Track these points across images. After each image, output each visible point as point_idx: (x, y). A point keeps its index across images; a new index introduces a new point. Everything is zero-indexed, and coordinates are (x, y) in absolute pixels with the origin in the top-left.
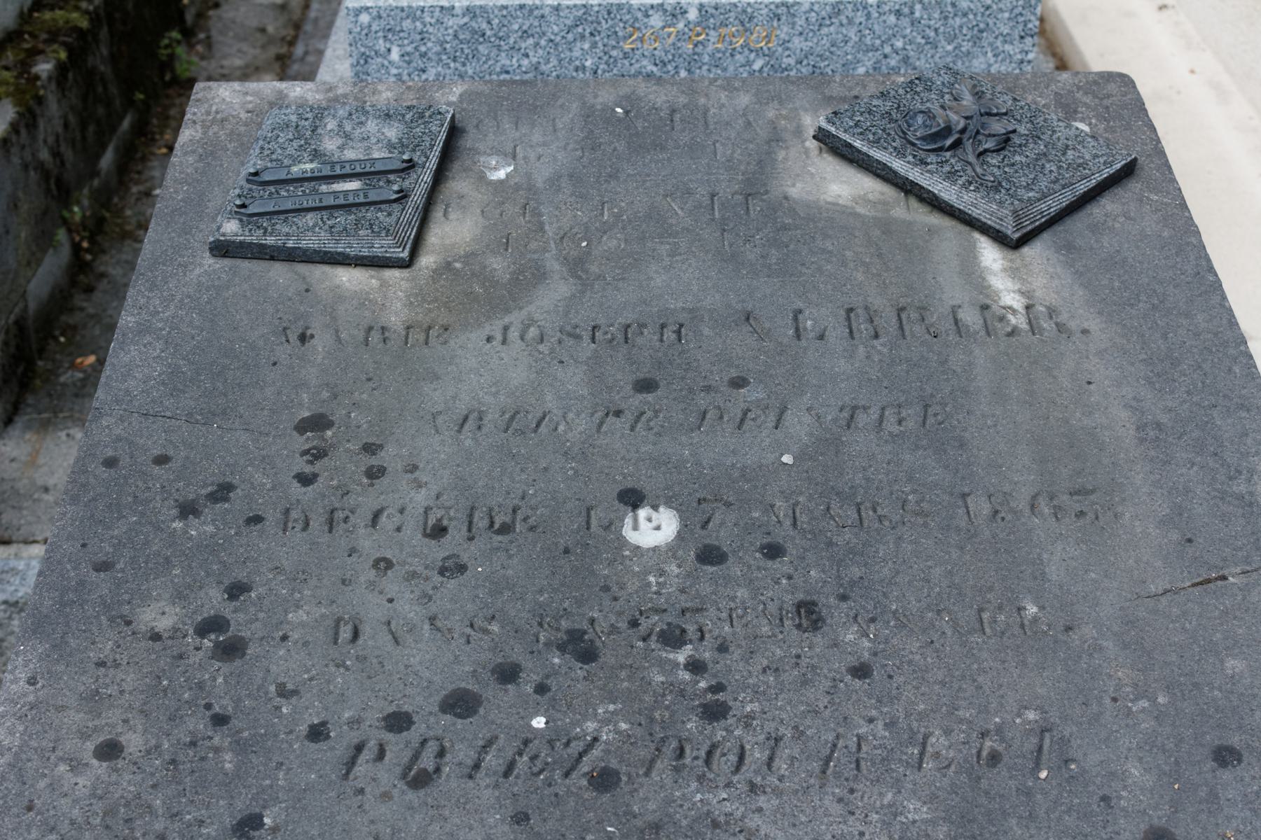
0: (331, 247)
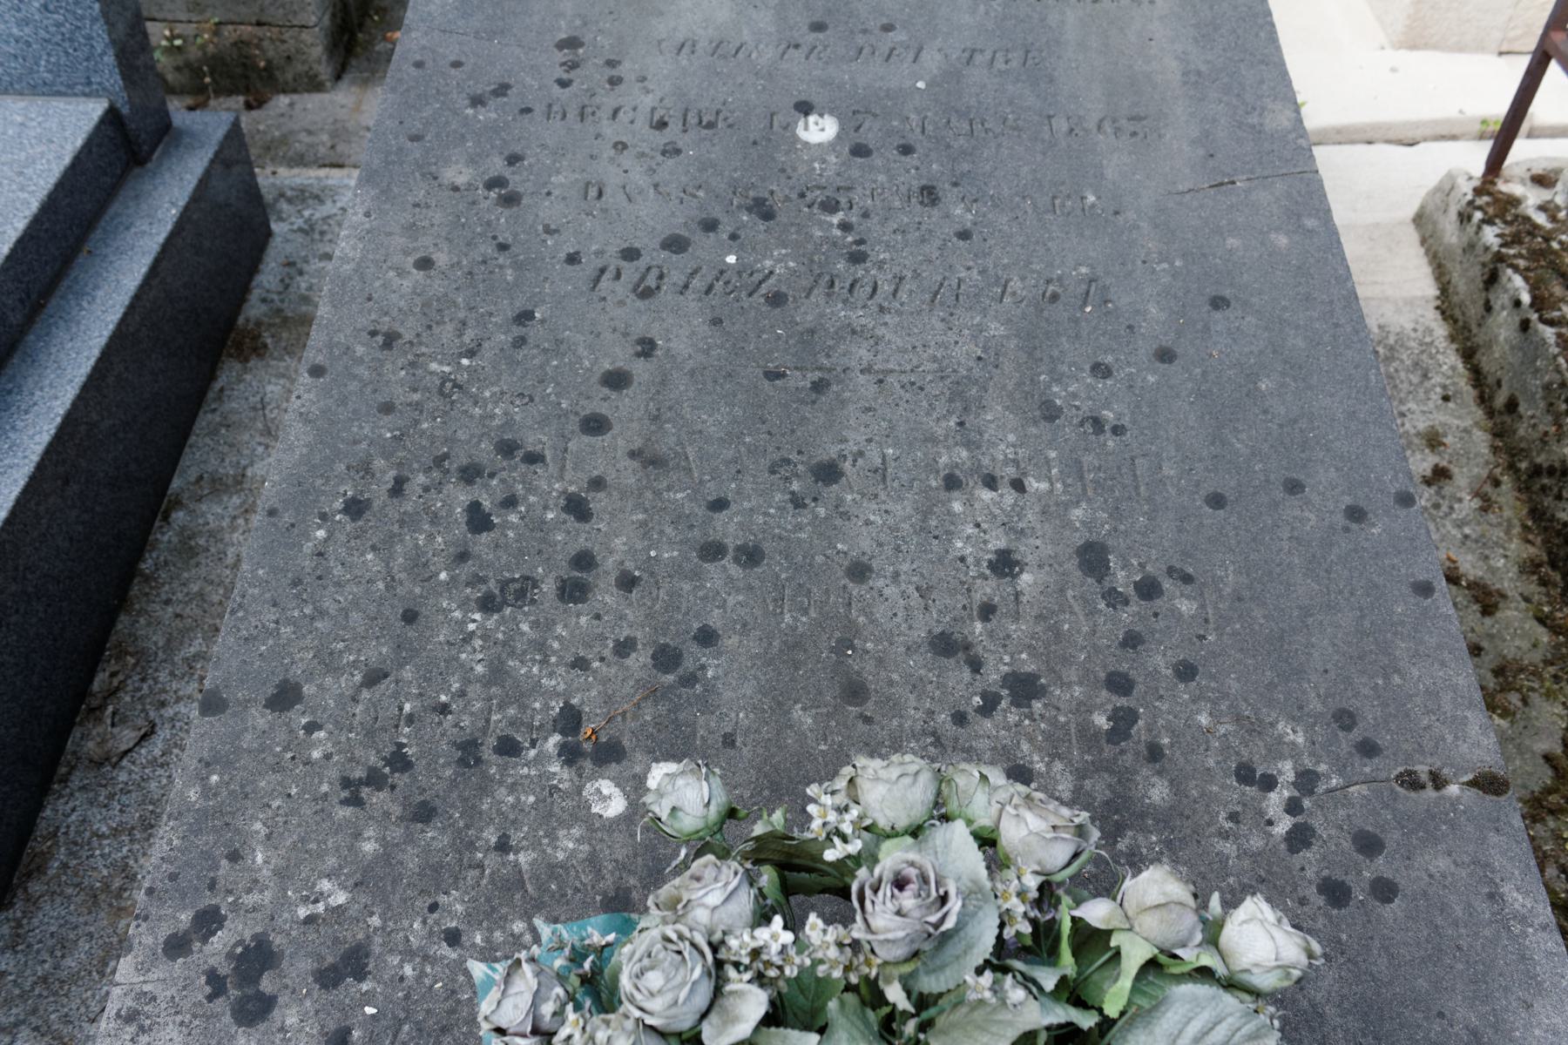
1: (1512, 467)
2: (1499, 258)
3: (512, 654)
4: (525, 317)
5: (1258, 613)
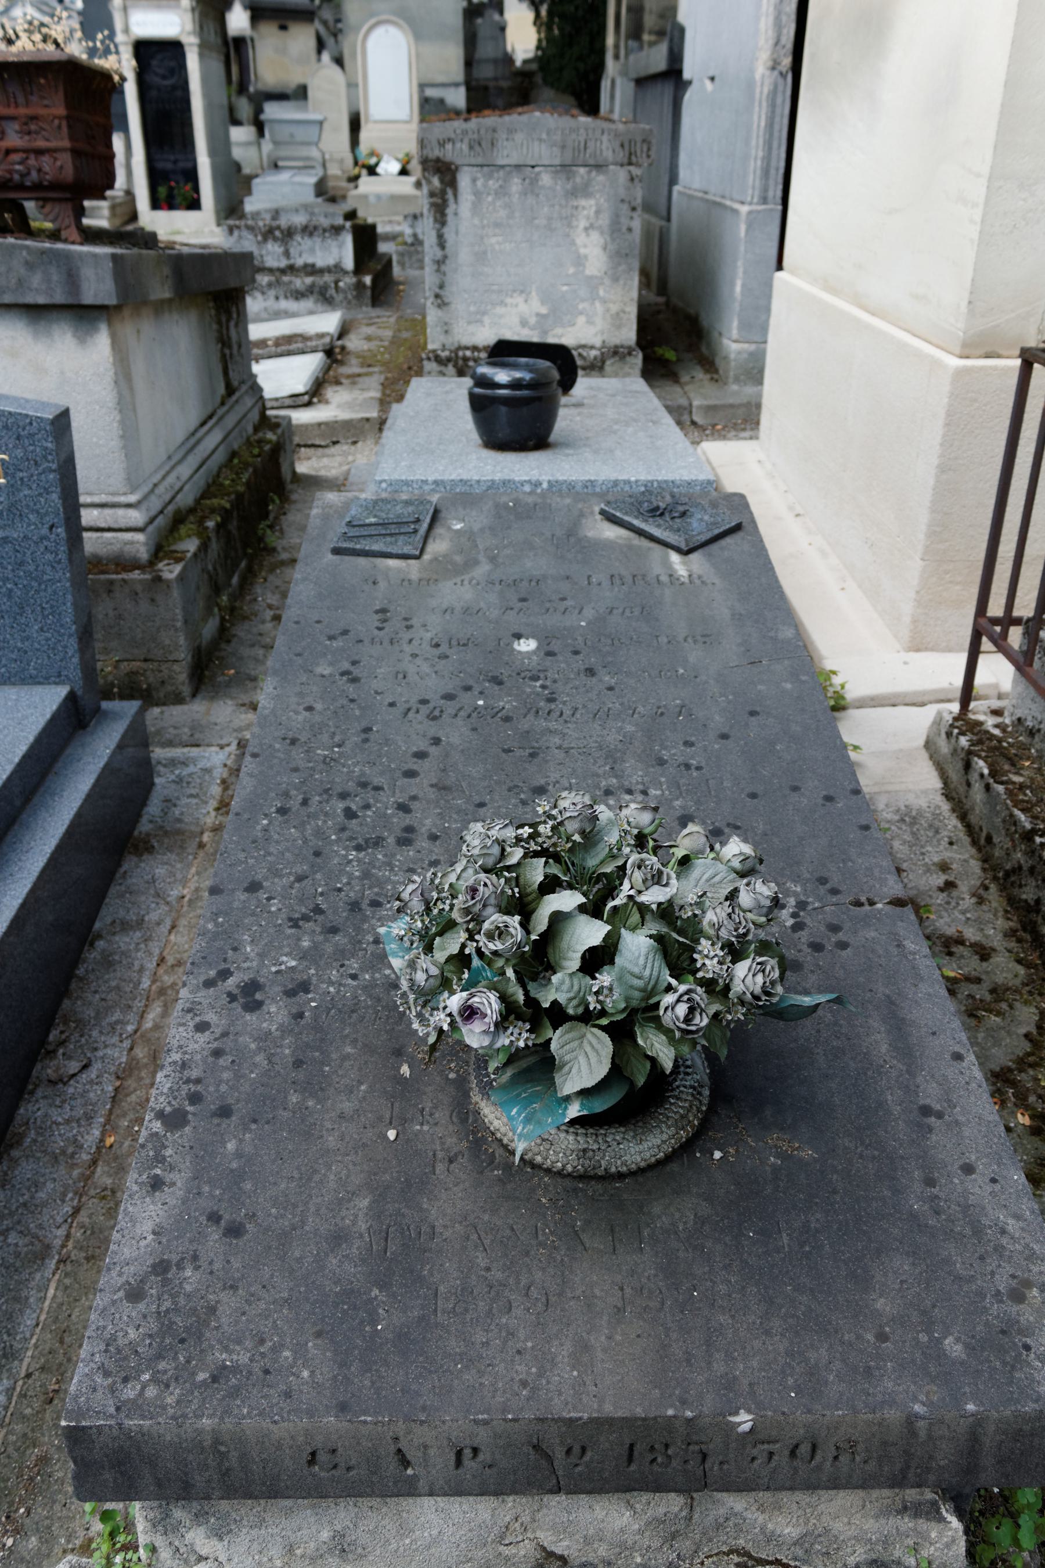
0: (385, 549)
1: (995, 878)
2: (969, 753)
3: (374, 867)
4: (368, 730)
5: (776, 840)
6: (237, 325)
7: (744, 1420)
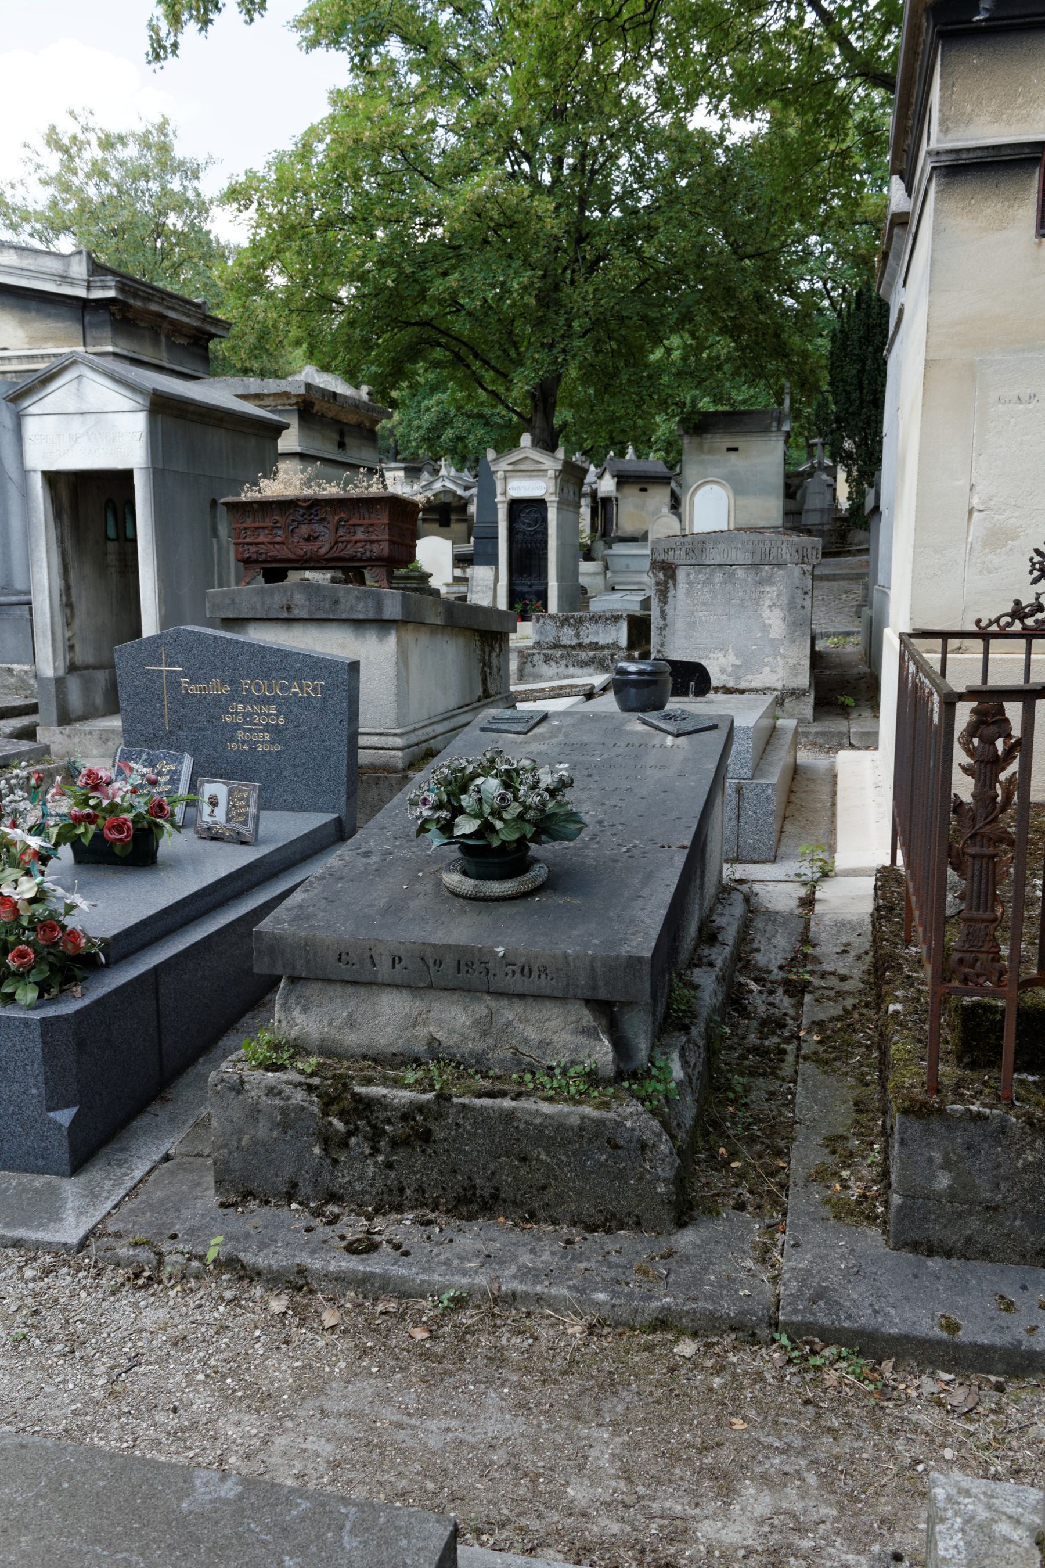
6: (498, 656)
7: (500, 950)
